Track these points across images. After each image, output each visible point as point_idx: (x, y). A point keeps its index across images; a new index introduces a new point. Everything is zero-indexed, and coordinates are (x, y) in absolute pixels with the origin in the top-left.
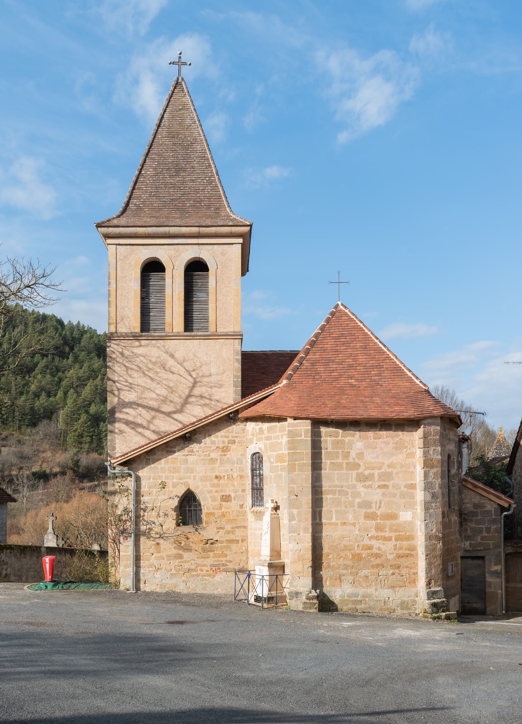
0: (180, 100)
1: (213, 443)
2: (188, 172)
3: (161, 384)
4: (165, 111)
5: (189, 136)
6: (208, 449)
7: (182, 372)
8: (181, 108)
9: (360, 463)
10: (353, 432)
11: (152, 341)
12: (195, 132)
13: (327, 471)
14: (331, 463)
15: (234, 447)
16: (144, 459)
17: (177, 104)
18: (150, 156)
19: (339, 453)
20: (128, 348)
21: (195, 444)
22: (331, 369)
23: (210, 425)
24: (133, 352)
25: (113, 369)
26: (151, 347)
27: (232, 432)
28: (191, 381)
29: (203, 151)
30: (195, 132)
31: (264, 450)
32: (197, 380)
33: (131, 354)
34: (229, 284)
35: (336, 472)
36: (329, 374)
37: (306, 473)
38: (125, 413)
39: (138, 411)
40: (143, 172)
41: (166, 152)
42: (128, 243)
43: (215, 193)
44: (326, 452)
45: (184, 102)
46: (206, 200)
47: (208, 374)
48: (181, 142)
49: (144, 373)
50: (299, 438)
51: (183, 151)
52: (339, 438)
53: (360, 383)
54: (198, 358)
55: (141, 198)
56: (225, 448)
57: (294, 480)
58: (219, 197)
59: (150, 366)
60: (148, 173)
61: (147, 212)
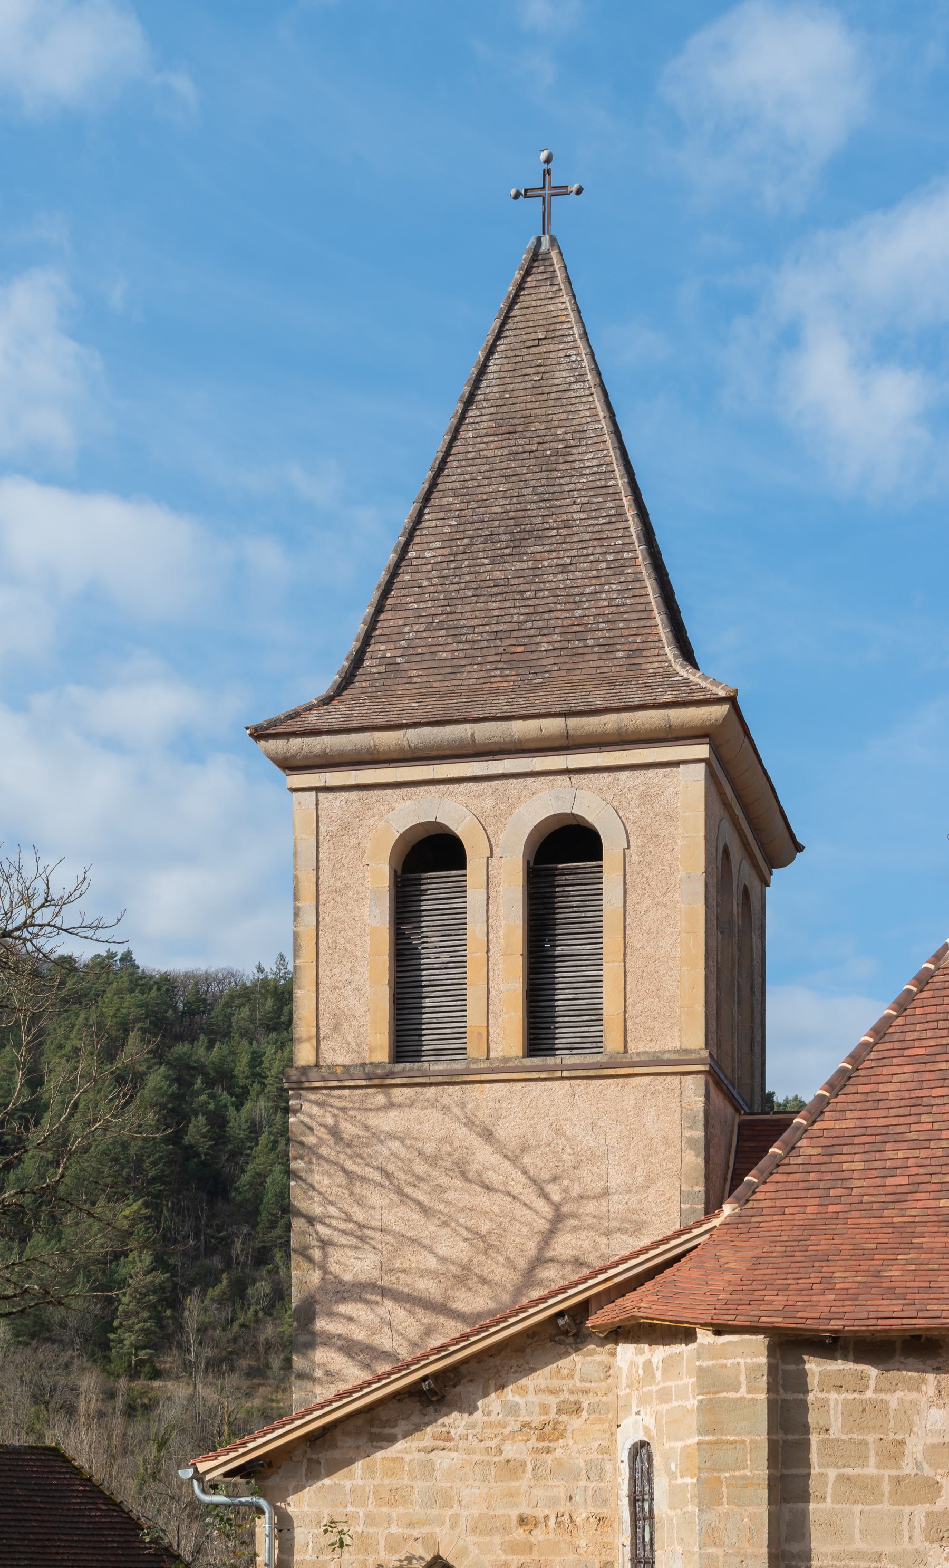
0: (540, 310)
1: (513, 1410)
2: (550, 541)
3: (453, 1224)
4: (491, 352)
5: (561, 423)
6: (497, 1431)
7: (519, 1184)
8: (540, 336)
9: (938, 1478)
10: (915, 1374)
11: (426, 1089)
12: (581, 407)
13: (829, 1504)
14: (840, 1477)
15: (575, 1423)
16: (301, 1461)
17: (531, 324)
18: (437, 502)
19: (866, 1444)
20: (351, 1113)
21: (455, 1415)
22: (889, 1164)
23: (503, 1354)
24: (366, 1127)
25: (309, 1181)
26: (422, 1108)
27: (571, 1376)
28: (545, 1214)
29: (604, 468)
30: (581, 407)
31: (654, 1433)
32: (565, 1209)
33: (361, 1133)
34: (665, 894)
35: (858, 1508)
36: (878, 1181)
37: (750, 1509)
38: (345, 1317)
39: (382, 1311)
40: (411, 554)
41: (486, 482)
42: (352, 782)
43: (632, 601)
44: (824, 1442)
45: (554, 314)
46: (601, 626)
47: (599, 1191)
48: (534, 447)
49: (400, 1192)
50: (732, 1395)
51: (538, 476)
52: (869, 1394)
53: (933, 1204)
54: (568, 1139)
55: (400, 637)
56: (548, 1428)
57: (716, 1534)
58: (644, 615)
59: (420, 1168)
60: (428, 554)
61: (415, 680)
